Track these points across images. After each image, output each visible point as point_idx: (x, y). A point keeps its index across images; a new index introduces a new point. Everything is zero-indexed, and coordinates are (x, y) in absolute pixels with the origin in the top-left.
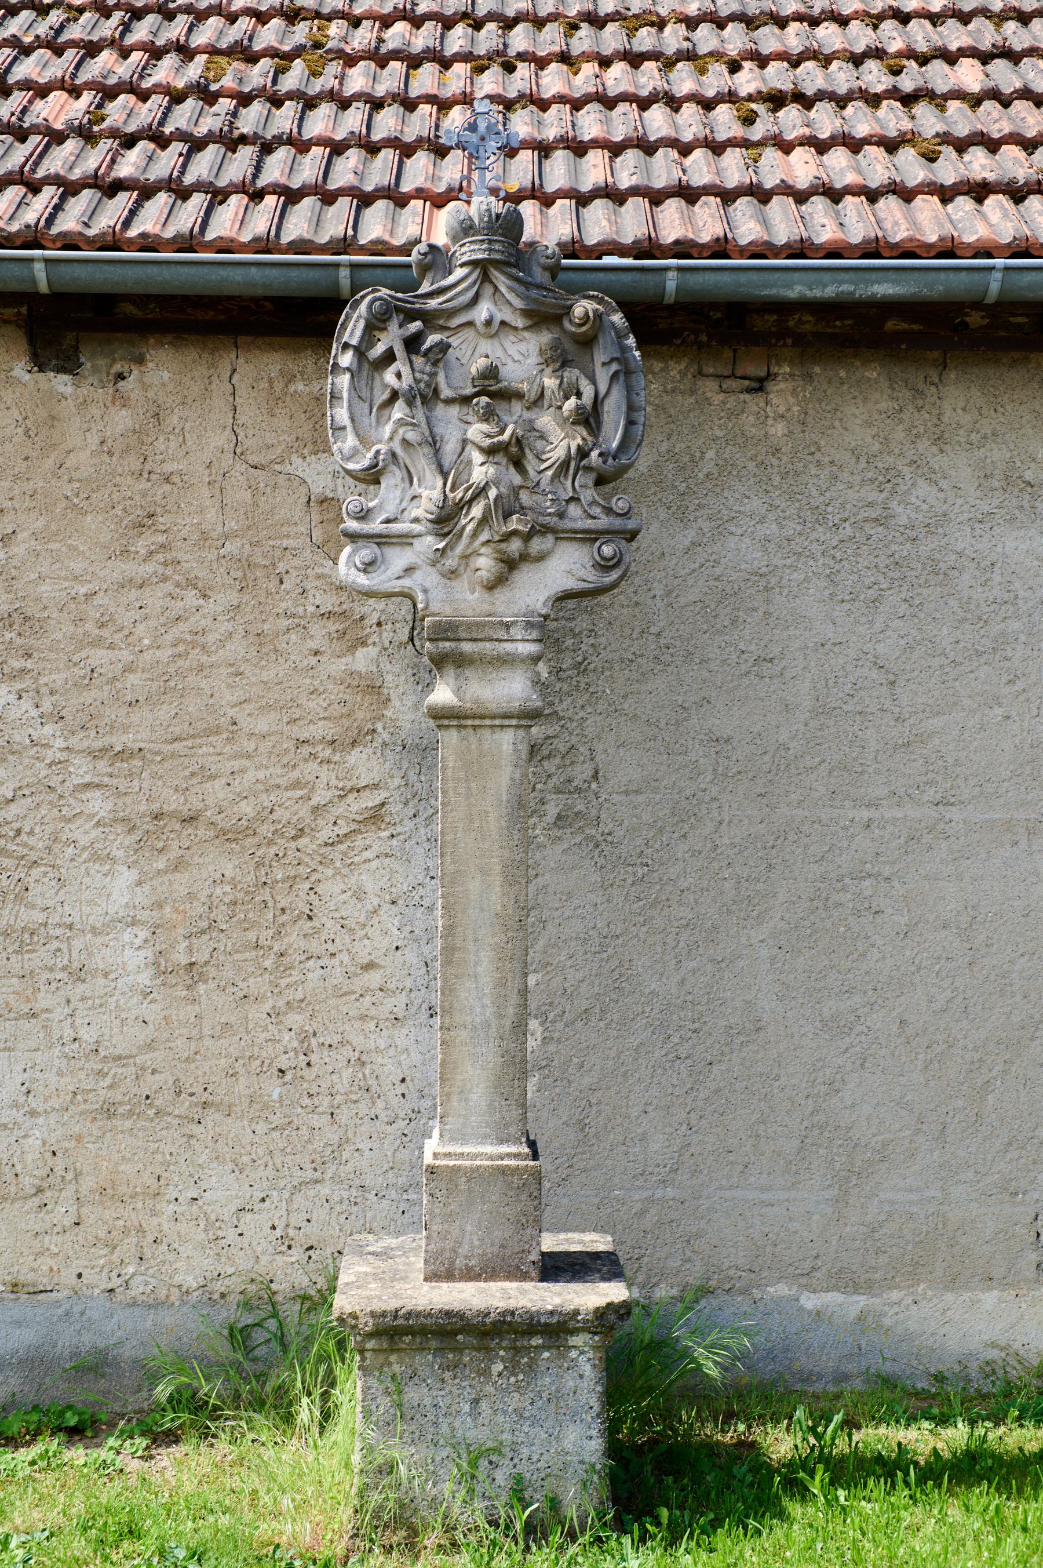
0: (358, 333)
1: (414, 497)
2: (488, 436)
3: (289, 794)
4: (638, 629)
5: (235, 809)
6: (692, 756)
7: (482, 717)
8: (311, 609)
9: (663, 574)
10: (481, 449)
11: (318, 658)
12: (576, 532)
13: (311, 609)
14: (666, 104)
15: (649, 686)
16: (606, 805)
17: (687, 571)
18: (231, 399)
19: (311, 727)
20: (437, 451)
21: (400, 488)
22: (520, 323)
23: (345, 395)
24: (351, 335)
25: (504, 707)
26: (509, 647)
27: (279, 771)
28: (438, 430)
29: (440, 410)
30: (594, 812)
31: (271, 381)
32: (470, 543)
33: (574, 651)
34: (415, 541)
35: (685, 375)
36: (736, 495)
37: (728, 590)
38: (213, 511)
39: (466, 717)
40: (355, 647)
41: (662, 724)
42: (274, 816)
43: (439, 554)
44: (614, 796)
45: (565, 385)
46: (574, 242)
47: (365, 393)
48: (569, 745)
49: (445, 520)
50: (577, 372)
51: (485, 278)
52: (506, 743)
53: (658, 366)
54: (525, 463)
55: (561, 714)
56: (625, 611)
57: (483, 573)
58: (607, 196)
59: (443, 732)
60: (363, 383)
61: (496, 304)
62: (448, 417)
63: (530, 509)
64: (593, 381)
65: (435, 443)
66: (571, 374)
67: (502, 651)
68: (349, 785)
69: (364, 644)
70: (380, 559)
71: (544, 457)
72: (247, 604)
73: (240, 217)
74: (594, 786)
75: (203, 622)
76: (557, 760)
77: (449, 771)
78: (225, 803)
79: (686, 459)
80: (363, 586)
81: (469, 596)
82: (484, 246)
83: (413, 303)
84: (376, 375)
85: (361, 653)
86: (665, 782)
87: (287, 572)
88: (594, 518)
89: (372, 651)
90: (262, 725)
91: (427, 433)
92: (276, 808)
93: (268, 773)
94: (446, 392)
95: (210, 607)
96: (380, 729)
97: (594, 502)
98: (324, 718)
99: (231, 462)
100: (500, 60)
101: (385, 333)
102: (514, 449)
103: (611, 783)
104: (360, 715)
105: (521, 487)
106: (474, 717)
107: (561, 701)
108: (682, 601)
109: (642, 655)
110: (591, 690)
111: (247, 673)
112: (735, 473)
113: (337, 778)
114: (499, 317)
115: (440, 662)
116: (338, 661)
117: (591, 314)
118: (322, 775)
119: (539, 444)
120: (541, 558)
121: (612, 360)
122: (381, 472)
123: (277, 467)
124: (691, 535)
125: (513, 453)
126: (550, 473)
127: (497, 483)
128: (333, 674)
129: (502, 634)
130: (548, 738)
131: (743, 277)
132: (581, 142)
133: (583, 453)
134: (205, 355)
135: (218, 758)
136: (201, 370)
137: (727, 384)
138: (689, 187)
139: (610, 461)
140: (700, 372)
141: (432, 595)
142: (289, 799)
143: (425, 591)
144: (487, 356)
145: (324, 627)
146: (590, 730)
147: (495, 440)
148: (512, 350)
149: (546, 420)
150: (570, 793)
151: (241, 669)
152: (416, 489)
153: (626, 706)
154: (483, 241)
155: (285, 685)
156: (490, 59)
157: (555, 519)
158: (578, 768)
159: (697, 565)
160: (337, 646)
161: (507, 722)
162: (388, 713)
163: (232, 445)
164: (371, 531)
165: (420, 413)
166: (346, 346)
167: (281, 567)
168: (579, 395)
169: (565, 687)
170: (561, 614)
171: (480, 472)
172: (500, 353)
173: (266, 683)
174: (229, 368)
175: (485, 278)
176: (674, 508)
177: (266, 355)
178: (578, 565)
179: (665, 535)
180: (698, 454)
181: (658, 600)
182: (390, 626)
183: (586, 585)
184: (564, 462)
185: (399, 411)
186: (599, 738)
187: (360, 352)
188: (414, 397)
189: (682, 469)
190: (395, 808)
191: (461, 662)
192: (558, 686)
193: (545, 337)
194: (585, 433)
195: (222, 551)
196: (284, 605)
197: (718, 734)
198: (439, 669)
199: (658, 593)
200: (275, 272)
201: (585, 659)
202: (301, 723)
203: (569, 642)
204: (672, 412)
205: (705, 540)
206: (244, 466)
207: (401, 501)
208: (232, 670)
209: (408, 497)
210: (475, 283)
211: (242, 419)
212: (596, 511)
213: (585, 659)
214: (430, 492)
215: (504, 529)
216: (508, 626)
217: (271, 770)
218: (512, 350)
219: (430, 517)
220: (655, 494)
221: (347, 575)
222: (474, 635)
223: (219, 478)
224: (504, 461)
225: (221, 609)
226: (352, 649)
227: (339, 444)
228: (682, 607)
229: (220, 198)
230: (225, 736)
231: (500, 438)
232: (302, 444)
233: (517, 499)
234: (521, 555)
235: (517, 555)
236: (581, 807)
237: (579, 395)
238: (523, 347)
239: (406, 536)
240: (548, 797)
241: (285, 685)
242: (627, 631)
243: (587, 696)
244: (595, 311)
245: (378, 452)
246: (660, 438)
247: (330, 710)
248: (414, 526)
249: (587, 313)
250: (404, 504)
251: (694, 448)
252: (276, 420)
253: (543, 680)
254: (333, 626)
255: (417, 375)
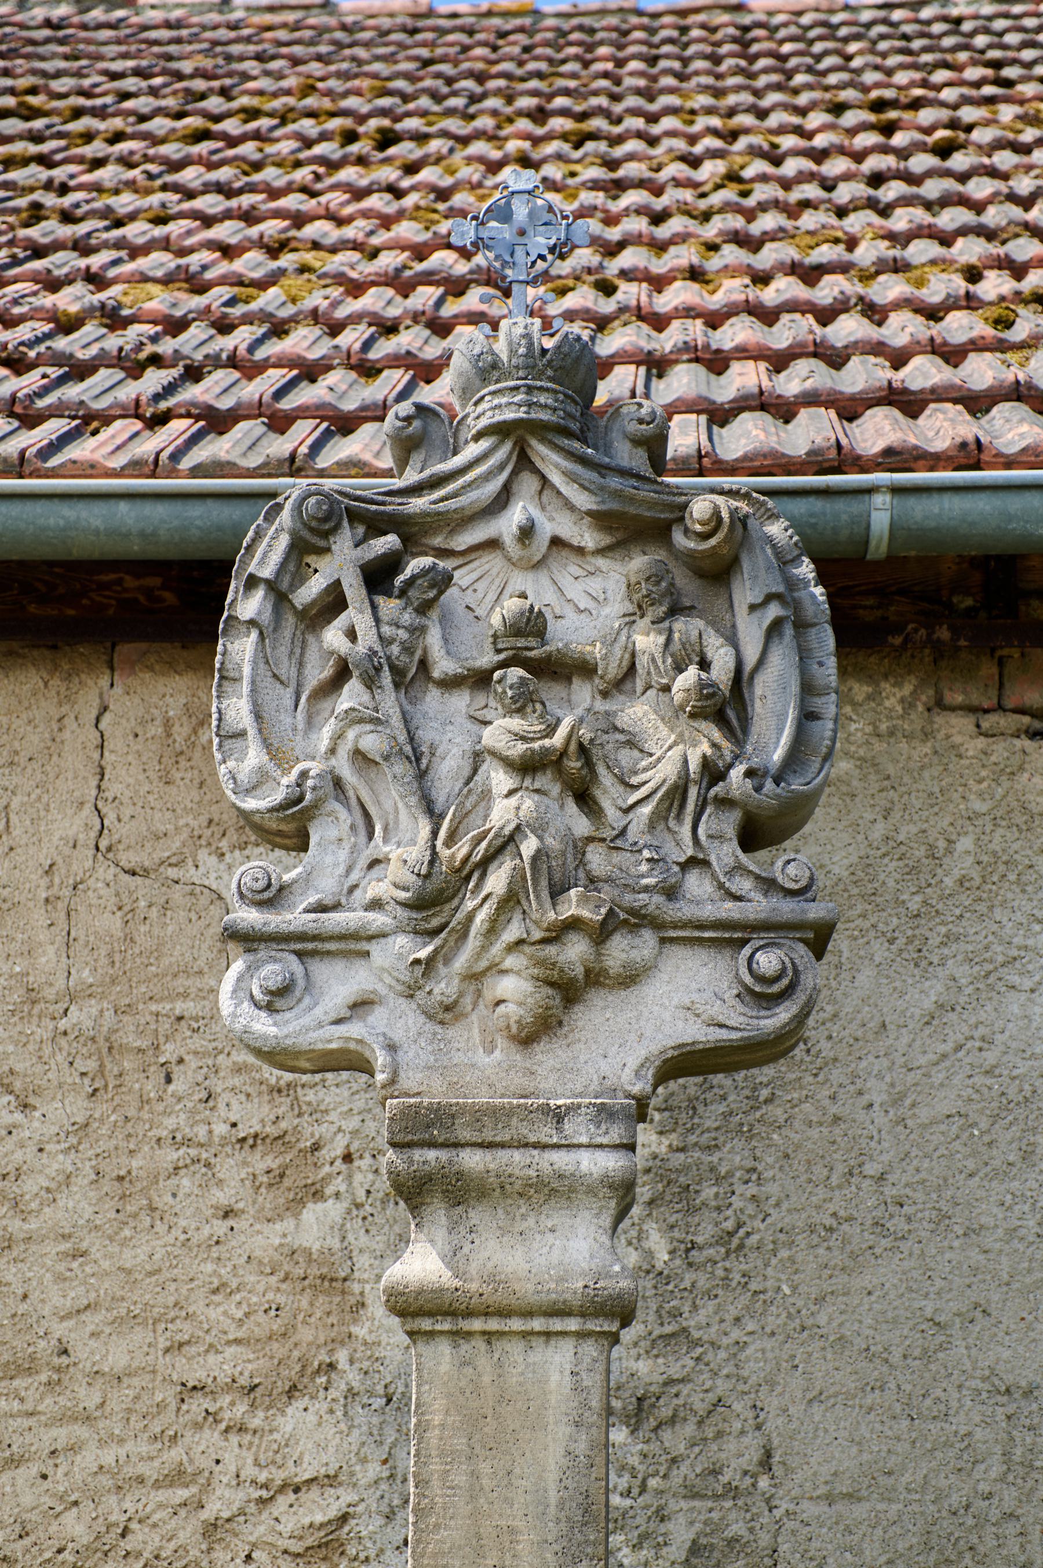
0: (276, 557)
1: (374, 863)
2: (524, 739)
3: (162, 1495)
4: (841, 1169)
5: (53, 1528)
6: (960, 1424)
7: (504, 1313)
8: (221, 1129)
9: (885, 1062)
10: (508, 763)
11: (230, 1222)
12: (701, 926)
13: (221, 1129)
14: (864, 313)
15: (867, 1280)
16: (790, 1525)
17: (931, 1057)
18: (96, 755)
19: (211, 1358)
20: (422, 775)
21: (347, 846)
22: (589, 538)
23: (247, 670)
24: (262, 562)
25: (552, 1292)
26: (561, 1159)
27: (144, 1448)
28: (426, 735)
29: (432, 699)
30: (765, 1539)
31: (168, 724)
32: (484, 948)
33: (718, 1209)
34: (374, 948)
35: (912, 706)
36: (1018, 917)
37: (1012, 1093)
38: (51, 950)
39: (469, 1314)
40: (302, 1202)
41: (896, 1357)
42: (129, 1544)
43: (419, 970)
44: (805, 1504)
45: (676, 646)
46: (700, 457)
47: (286, 669)
48: (711, 1397)
49: (432, 902)
50: (700, 623)
51: (524, 461)
52: (556, 1370)
53: (860, 690)
54: (597, 793)
55: (696, 1334)
56: (814, 1133)
57: (510, 1009)
58: (763, 407)
59: (421, 1347)
60: (283, 651)
61: (543, 508)
62: (450, 725)
63: (609, 880)
64: (732, 640)
65: (418, 760)
66: (685, 627)
67: (545, 1166)
68: (279, 1476)
69: (318, 1195)
70: (301, 983)
71: (635, 780)
72: (102, 1121)
73: (119, 441)
74: (764, 1483)
75: (18, 1156)
76: (689, 1429)
77: (433, 1436)
78: (34, 1516)
79: (920, 852)
80: (265, 1037)
81: (481, 1058)
82: (519, 398)
83: (383, 503)
84: (311, 638)
85: (312, 1212)
86: (907, 1477)
87: (181, 1061)
88: (739, 898)
89: (333, 1210)
90: (117, 1358)
91: (402, 738)
92: (134, 1525)
93: (122, 1452)
94: (443, 666)
95: (33, 1127)
96: (343, 1363)
97: (738, 868)
98: (237, 1341)
99: (89, 864)
100: (591, 279)
101: (327, 558)
102: (573, 764)
103: (798, 1477)
104: (305, 1334)
105: (590, 839)
106: (486, 1313)
107: (695, 1307)
108: (924, 1114)
109: (850, 1219)
110: (753, 1286)
111: (95, 1253)
112: (1012, 877)
113: (257, 1463)
114: (547, 528)
115: (414, 1192)
116: (267, 1228)
117: (725, 515)
118: (227, 1457)
119: (626, 757)
120: (631, 978)
121: (769, 598)
122: (308, 815)
123: (172, 873)
124: (934, 990)
125: (572, 773)
126: (646, 810)
127: (539, 829)
128: (258, 1253)
129: (546, 1133)
130: (670, 1382)
131: (1015, 503)
132: (718, 351)
133: (713, 773)
134: (55, 682)
135: (27, 1422)
136: (47, 707)
137: (988, 722)
138: (905, 391)
139: (769, 785)
140: (940, 705)
141: (408, 1056)
142: (161, 1506)
143: (392, 1048)
144: (523, 596)
145: (245, 1163)
146: (753, 1368)
147: (536, 745)
148: (575, 591)
149: (637, 712)
150: (716, 1497)
151: (84, 1245)
152: (379, 846)
153: (822, 1319)
154: (516, 388)
155: (166, 1274)
156: (577, 278)
157: (658, 899)
158: (731, 1445)
159: (948, 1047)
160: (267, 1199)
161: (557, 1325)
162: (360, 1331)
163: (93, 834)
164: (284, 928)
165: (389, 701)
166: (252, 582)
167: (169, 1052)
168: (704, 665)
169: (703, 1281)
170: (692, 1139)
171: (506, 804)
172: (549, 596)
173: (129, 1272)
174: (96, 703)
175: (524, 461)
176: (901, 942)
177: (162, 680)
178: (708, 995)
179: (885, 990)
180: (942, 844)
181: (877, 1111)
182: (368, 1160)
183: (724, 1034)
184: (675, 788)
185: (352, 695)
186: (772, 1384)
187: (279, 594)
188: (378, 670)
189: (913, 870)
190: (366, 1526)
191: (460, 1192)
192: (689, 1277)
193: (639, 562)
194: (717, 735)
195: (63, 1024)
196: (170, 1122)
197: (1009, 1379)
198: (415, 1209)
199: (878, 1098)
200: (159, 511)
201: (739, 1226)
202: (192, 1350)
203: (708, 1192)
204: (891, 770)
205: (962, 1000)
206: (113, 870)
207: (349, 870)
208: (65, 1246)
209: (363, 862)
210: (501, 467)
211: (113, 789)
212: (743, 885)
213: (739, 1226)
214: (407, 847)
215: (552, 915)
216: (559, 1116)
217: (129, 1446)
218: (575, 591)
219: (403, 895)
220: (864, 916)
221: (234, 1015)
222: (488, 1136)
223: (66, 892)
224: (556, 789)
225: (55, 1129)
226: (295, 1205)
227: (231, 764)
228: (924, 1126)
229: (95, 424)
230: (43, 1377)
231: (547, 742)
232: (218, 831)
233: (582, 863)
234: (588, 972)
235: (579, 971)
236: (737, 1528)
237: (704, 665)
238: (595, 585)
239: (354, 936)
240: (673, 1505)
241: (166, 1274)
242: (819, 1171)
243: (745, 1299)
244: (733, 512)
245: (304, 775)
246: (869, 816)
247: (249, 1324)
248: (371, 915)
249: (716, 514)
250: (354, 876)
251: (933, 834)
252: (172, 790)
253: (659, 1265)
254: (262, 1162)
255: (386, 630)
